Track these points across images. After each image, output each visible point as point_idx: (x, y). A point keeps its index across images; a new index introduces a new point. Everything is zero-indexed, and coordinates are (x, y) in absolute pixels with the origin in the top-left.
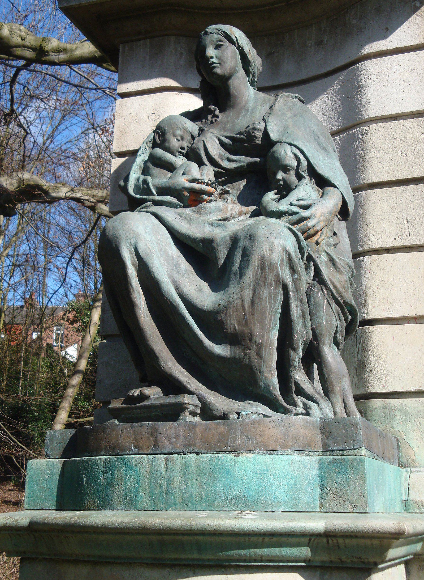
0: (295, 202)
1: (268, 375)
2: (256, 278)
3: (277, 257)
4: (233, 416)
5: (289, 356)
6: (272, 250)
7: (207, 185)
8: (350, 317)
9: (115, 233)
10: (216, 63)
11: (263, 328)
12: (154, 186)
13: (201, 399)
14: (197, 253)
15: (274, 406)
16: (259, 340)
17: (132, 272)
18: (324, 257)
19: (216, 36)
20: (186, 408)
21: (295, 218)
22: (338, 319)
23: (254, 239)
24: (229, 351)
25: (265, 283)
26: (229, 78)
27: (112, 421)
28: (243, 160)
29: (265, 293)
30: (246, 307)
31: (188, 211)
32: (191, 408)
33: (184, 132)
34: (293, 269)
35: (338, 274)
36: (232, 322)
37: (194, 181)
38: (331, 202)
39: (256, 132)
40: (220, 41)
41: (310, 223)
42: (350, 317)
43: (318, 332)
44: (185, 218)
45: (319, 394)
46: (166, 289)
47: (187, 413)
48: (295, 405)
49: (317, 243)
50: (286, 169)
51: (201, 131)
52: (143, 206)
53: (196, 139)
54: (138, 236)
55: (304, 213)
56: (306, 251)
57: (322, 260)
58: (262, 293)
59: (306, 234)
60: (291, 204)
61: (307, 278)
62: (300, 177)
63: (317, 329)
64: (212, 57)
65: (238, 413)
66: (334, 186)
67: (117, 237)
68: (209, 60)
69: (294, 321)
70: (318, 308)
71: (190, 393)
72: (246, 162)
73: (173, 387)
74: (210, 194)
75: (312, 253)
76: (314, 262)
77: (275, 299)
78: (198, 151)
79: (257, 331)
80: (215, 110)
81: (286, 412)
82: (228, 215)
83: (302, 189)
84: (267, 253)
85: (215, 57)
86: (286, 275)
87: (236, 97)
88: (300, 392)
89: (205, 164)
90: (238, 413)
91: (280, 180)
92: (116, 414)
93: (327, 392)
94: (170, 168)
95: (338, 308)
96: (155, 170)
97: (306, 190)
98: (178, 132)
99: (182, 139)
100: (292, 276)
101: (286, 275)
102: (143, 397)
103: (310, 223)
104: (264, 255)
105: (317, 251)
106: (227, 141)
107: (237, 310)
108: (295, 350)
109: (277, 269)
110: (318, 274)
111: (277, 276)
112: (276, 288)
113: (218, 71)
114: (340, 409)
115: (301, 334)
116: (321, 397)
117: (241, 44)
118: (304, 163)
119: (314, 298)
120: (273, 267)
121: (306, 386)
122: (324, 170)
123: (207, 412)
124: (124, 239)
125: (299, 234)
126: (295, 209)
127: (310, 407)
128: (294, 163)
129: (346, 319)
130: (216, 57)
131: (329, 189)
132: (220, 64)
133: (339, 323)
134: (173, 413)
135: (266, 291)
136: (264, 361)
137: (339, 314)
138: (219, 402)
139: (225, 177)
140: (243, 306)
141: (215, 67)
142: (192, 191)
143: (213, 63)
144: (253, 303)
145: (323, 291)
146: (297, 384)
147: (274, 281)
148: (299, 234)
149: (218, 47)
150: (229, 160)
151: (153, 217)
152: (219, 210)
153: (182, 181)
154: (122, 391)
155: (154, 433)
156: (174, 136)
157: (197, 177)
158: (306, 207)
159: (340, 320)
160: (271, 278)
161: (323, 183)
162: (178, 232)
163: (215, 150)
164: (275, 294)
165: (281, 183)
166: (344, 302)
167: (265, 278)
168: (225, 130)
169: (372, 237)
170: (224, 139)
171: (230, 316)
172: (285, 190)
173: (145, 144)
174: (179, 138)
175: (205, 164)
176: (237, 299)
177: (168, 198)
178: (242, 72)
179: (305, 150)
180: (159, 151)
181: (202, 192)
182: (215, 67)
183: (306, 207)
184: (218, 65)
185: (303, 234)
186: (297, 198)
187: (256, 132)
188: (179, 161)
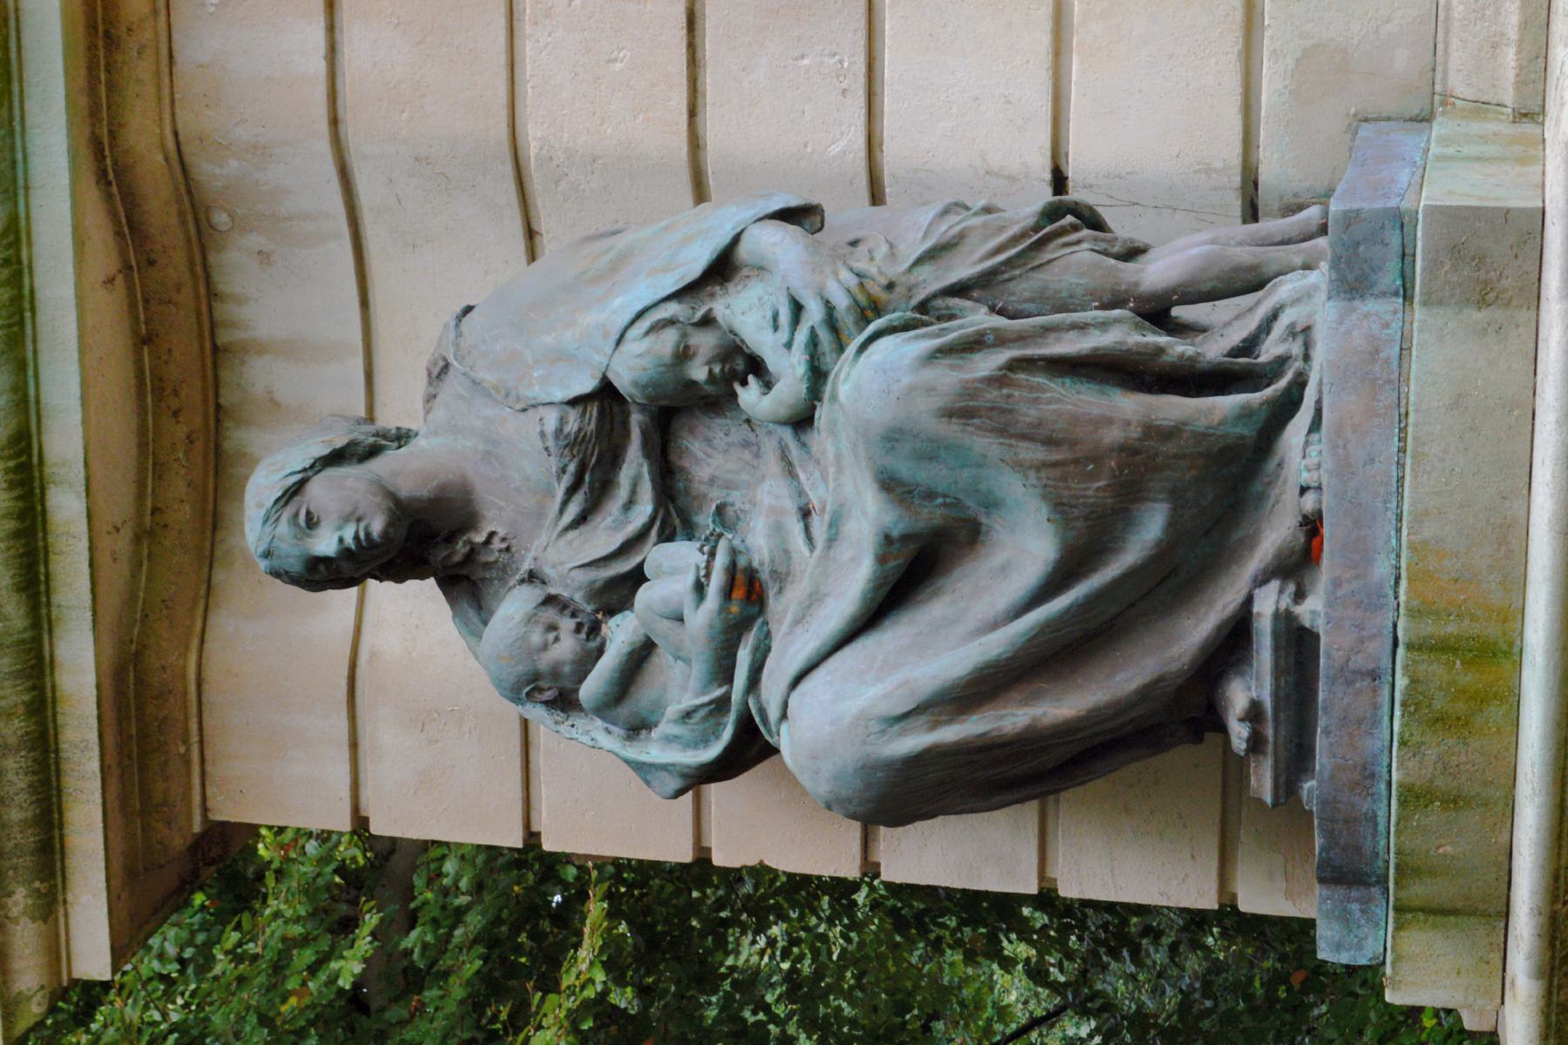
0: (783, 335)
1: (1216, 418)
2: (992, 430)
3: (948, 377)
4: (1309, 502)
5: (1173, 366)
6: (930, 390)
7: (712, 554)
8: (1070, 219)
9: (850, 770)
10: (357, 533)
11: (1109, 421)
12: (703, 693)
13: (1261, 580)
14: (912, 573)
15: (1288, 404)
16: (1135, 433)
17: (951, 733)
18: (925, 271)
19: (284, 527)
20: (1288, 613)
21: (824, 336)
22: (1076, 248)
23: (901, 430)
24: (1157, 506)
25: (1003, 411)
26: (392, 496)
27: (1304, 793)
28: (634, 466)
29: (1029, 413)
30: (1056, 456)
31: (774, 605)
32: (1286, 601)
33: (537, 622)
34: (974, 344)
35: (967, 240)
36: (1090, 493)
37: (700, 588)
38: (777, 246)
39: (567, 429)
40: (296, 515)
41: (841, 302)
42: (1070, 219)
43: (1107, 298)
44: (809, 606)
45: (1258, 303)
46: (1000, 650)
47: (1298, 610)
48: (1282, 361)
49: (890, 286)
50: (683, 355)
51: (532, 577)
52: (757, 720)
53: (553, 591)
54: (863, 717)
55: (814, 313)
56: (909, 314)
57: (933, 280)
58: (1028, 420)
59: (869, 314)
60: (789, 345)
61: (977, 318)
62: (707, 321)
63: (1100, 299)
64: (341, 540)
65: (1304, 490)
66: (736, 240)
67: (863, 767)
68: (348, 550)
69: (1096, 349)
70: (1048, 293)
71: (1249, 600)
72: (641, 460)
73: (1234, 640)
74: (734, 553)
75: (914, 302)
76: (935, 296)
77: (1040, 388)
78: (598, 585)
79: (1113, 435)
80: (470, 542)
81: (1300, 383)
82: (790, 505)
83: (743, 318)
84: (936, 402)
85: (338, 533)
86: (988, 363)
87: (443, 487)
88: (1249, 346)
89: (640, 566)
90: (1304, 490)
91: (710, 372)
92: (1287, 786)
93: (1251, 282)
94: (642, 654)
95: (1052, 245)
96: (643, 697)
97: (746, 312)
98: (536, 638)
99: (552, 627)
100: (989, 346)
101: (988, 363)
102: (1254, 714)
103: (841, 302)
104: (939, 409)
105: (910, 289)
106: (573, 510)
107: (1064, 479)
108: (1160, 350)
109: (974, 380)
110: (960, 290)
111: (991, 381)
112: (1018, 386)
113: (377, 526)
114: (1295, 254)
115: (1120, 334)
116: (1265, 297)
117: (307, 464)
118: (672, 309)
119: (1025, 301)
120: (970, 391)
121: (1236, 336)
122: (697, 260)
123: (1297, 565)
124: (870, 749)
125: (872, 328)
126: (802, 336)
127: (1292, 326)
128: (670, 338)
129: (1075, 228)
130: (340, 528)
131: (744, 251)
132: (359, 520)
133: (1085, 246)
134: (1298, 644)
135: (1023, 408)
136: (1185, 424)
137: (1065, 245)
138: (1275, 534)
139: (673, 515)
140: (1055, 465)
141: (368, 535)
142: (727, 592)
143: (356, 538)
144: (1050, 442)
145: (1010, 280)
146: (1236, 352)
147: (1000, 388)
148: (872, 328)
149: (312, 523)
150: (630, 504)
151: (805, 686)
152: (778, 529)
153: (703, 617)
154: (1234, 770)
155: (1346, 676)
156: (545, 647)
157: (690, 579)
158: (797, 308)
159: (1079, 242)
160: (993, 395)
161: (723, 269)
162: (854, 620)
163: (604, 536)
164: (1031, 388)
165: (717, 369)
166: (1036, 228)
167: (992, 409)
168: (540, 514)
169: (835, 149)
170: (568, 517)
171: (1078, 498)
172: (745, 364)
173: (562, 728)
174: (551, 636)
175: (640, 566)
176: (1039, 479)
177: (744, 657)
178: (377, 465)
179: (640, 307)
180: (592, 687)
181: (732, 570)
182: (368, 535)
183: (797, 308)
184: (362, 525)
185: (869, 322)
186: (770, 330)
187: (567, 429)
188: (621, 633)
